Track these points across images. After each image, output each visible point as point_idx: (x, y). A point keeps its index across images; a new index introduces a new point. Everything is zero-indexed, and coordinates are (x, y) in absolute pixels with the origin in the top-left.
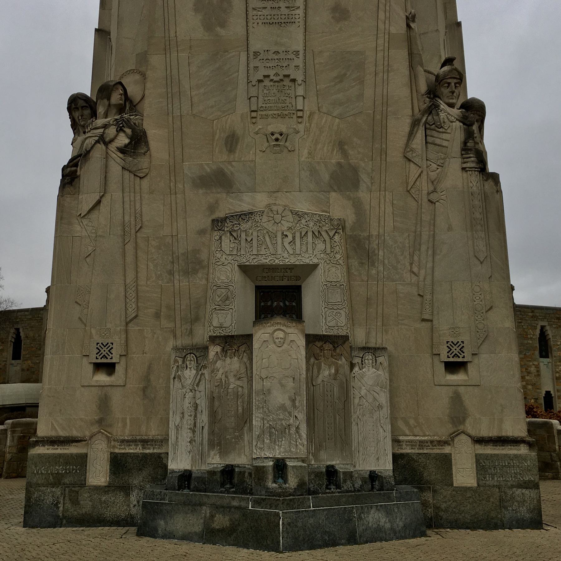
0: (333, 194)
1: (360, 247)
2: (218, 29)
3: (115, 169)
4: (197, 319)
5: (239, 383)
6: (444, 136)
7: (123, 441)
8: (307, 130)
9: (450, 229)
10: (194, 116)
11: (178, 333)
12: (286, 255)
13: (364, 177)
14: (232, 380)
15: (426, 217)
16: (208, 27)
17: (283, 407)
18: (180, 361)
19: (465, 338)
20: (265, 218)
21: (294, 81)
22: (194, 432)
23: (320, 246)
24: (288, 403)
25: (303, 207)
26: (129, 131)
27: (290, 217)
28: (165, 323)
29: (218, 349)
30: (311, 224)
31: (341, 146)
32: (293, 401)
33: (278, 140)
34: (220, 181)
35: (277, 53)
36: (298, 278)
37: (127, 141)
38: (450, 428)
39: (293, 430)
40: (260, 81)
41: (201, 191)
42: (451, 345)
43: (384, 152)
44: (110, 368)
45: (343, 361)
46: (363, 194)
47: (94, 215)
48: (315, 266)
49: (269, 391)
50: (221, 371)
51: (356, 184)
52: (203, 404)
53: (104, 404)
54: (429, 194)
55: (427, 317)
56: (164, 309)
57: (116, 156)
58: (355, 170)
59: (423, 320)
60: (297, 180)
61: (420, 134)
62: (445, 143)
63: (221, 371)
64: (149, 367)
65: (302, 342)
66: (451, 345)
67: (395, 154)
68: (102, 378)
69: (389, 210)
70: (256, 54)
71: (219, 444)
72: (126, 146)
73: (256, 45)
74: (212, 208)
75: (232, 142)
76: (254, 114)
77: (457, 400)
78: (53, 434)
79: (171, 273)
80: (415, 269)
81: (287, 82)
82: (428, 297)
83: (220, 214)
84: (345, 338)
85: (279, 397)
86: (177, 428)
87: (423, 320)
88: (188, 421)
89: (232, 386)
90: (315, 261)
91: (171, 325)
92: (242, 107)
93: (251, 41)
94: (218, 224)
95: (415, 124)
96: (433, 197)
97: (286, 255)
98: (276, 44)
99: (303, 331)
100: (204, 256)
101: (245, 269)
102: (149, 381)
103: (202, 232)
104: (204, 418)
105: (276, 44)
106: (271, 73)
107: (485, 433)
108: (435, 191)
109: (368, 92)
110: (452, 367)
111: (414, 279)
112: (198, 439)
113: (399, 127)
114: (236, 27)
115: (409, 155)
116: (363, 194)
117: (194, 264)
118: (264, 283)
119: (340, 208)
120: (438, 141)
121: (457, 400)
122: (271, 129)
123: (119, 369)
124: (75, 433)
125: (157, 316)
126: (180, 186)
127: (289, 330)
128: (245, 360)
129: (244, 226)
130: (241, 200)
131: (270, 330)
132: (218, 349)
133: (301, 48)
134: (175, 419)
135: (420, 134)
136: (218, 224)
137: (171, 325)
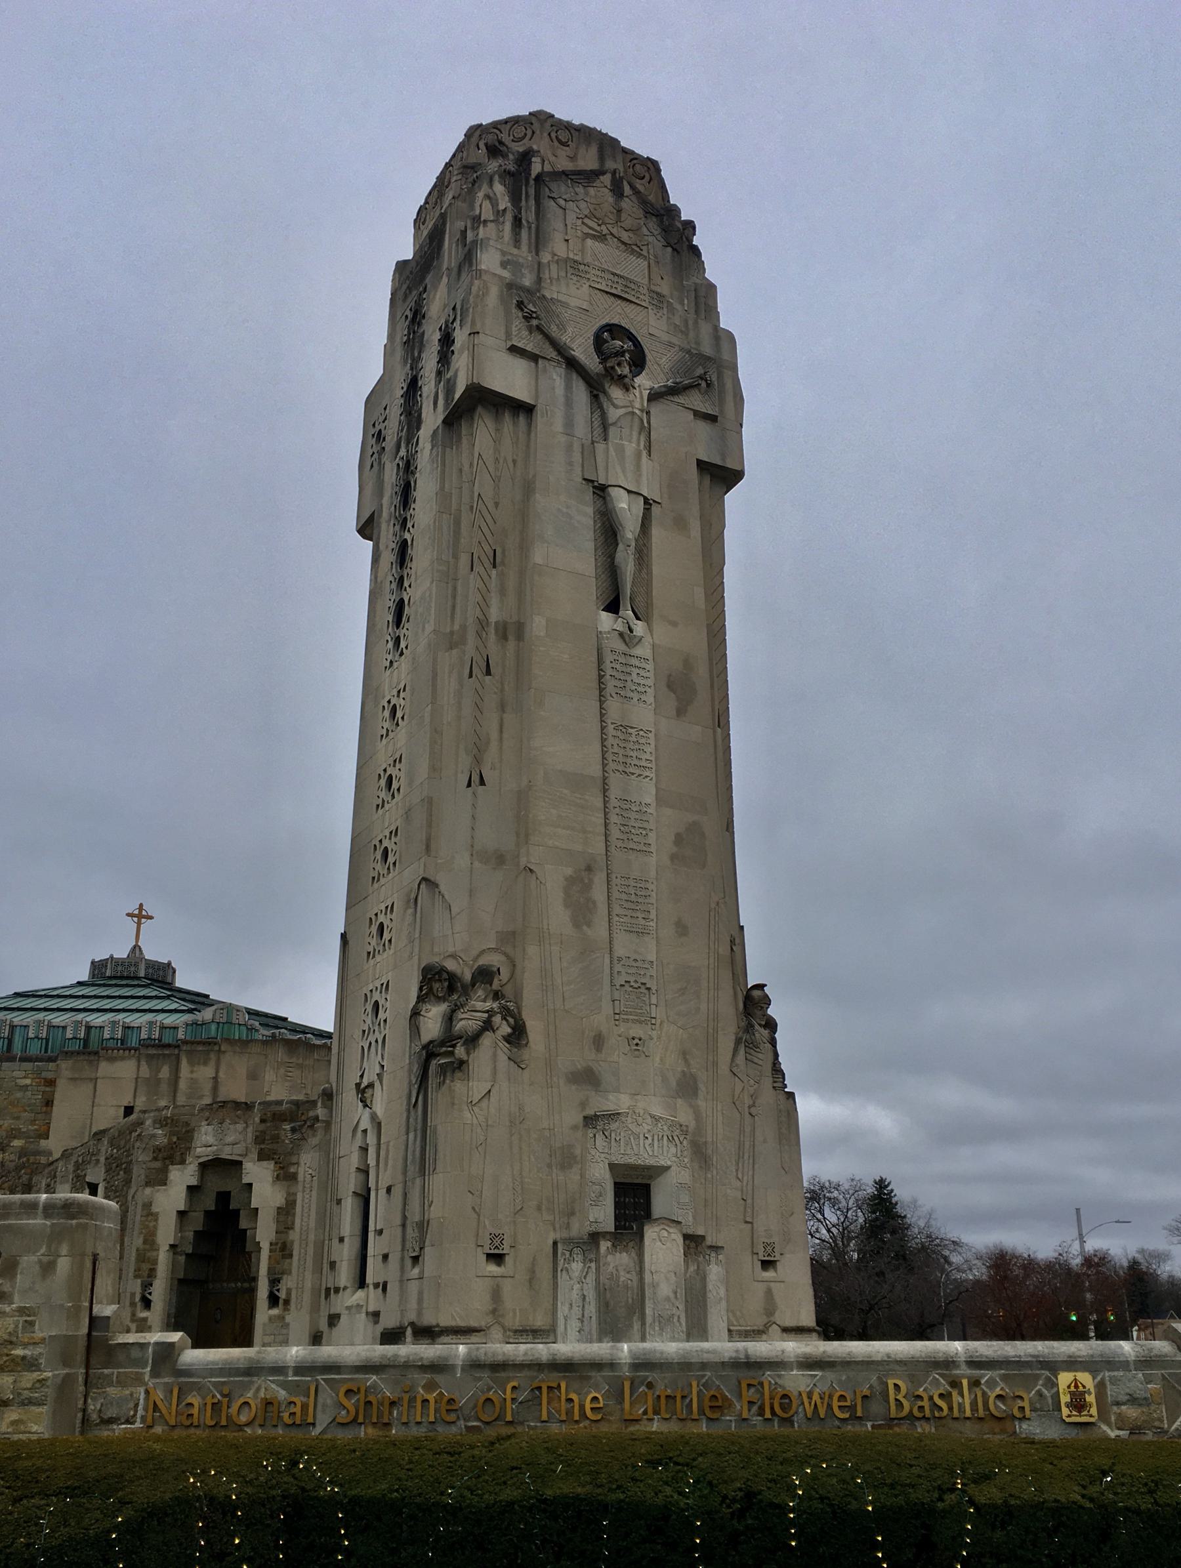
0: (679, 1101)
1: (701, 1154)
2: (585, 928)
3: (502, 1058)
4: (573, 1213)
5: (628, 1276)
6: (760, 1056)
7: (516, 1331)
8: (659, 1038)
9: (765, 1141)
10: (567, 1011)
11: (557, 1226)
12: (646, 1156)
13: (701, 1086)
14: (622, 1273)
15: (748, 1130)
16: (577, 925)
17: (668, 1299)
18: (568, 1254)
19: (775, 1239)
20: (629, 1120)
21: (649, 989)
22: (582, 1322)
23: (673, 1150)
24: (672, 1295)
25: (658, 1111)
26: (511, 1020)
27: (649, 1120)
28: (546, 1217)
29: (609, 1244)
30: (665, 1128)
31: (684, 1054)
32: (675, 1293)
33: (636, 1043)
34: (588, 1078)
35: (636, 960)
36: (650, 1177)
37: (509, 1030)
38: (765, 1320)
39: (675, 1319)
40: (622, 985)
41: (574, 1087)
42: (765, 1245)
43: (715, 1064)
44: (497, 1258)
45: (701, 1259)
46: (701, 1103)
47: (484, 1104)
48: (669, 1168)
49: (658, 1284)
50: (612, 1265)
51: (694, 1092)
52: (591, 1295)
53: (496, 1295)
54: (749, 1107)
55: (749, 1219)
56: (544, 1202)
57: (504, 1045)
58: (694, 1078)
59: (747, 1222)
60: (652, 1085)
61: (742, 1051)
62: (760, 1062)
63: (612, 1265)
64: (534, 1259)
65: (680, 1240)
66: (765, 1245)
67: (724, 1068)
68: (493, 1268)
69: (720, 1118)
70: (620, 959)
71: (612, 1332)
72: (509, 1035)
73: (619, 951)
74: (583, 1105)
75: (598, 1041)
76: (617, 1017)
77: (769, 1293)
78: (453, 1324)
79: (549, 1166)
80: (740, 1176)
81: (643, 990)
82: (749, 1201)
83: (590, 1112)
84: (703, 1237)
85: (665, 1290)
86: (566, 1318)
87: (747, 1222)
88: (576, 1311)
89: (622, 1279)
90: (669, 1163)
91: (551, 1218)
92: (607, 1008)
93: (616, 947)
94: (590, 1121)
95: (738, 1041)
96: (753, 1110)
97: (646, 1156)
98: (635, 952)
99: (681, 1231)
100: (578, 1152)
101: (612, 1166)
102: (534, 1272)
103: (575, 1128)
104: (591, 1309)
105: (635, 952)
106: (632, 979)
107: (789, 1323)
108: (753, 1105)
109: (703, 1007)
110: (767, 1264)
111: (739, 1183)
112: (586, 1329)
113: (726, 1043)
114: (599, 931)
115: (734, 1069)
116: (701, 1103)
117: (567, 1159)
118: (622, 1180)
119: (685, 1116)
120: (756, 1060)
121: (769, 1293)
122: (632, 1033)
123: (508, 1260)
124: (473, 1323)
125: (539, 1208)
126: (555, 1079)
127: (671, 1230)
128: (633, 1254)
129: (614, 1126)
130: (607, 1099)
131: (657, 1229)
132: (609, 1244)
133: (654, 958)
134: (563, 1310)
135: (742, 1051)
136: (590, 1121)
137: (551, 1218)
